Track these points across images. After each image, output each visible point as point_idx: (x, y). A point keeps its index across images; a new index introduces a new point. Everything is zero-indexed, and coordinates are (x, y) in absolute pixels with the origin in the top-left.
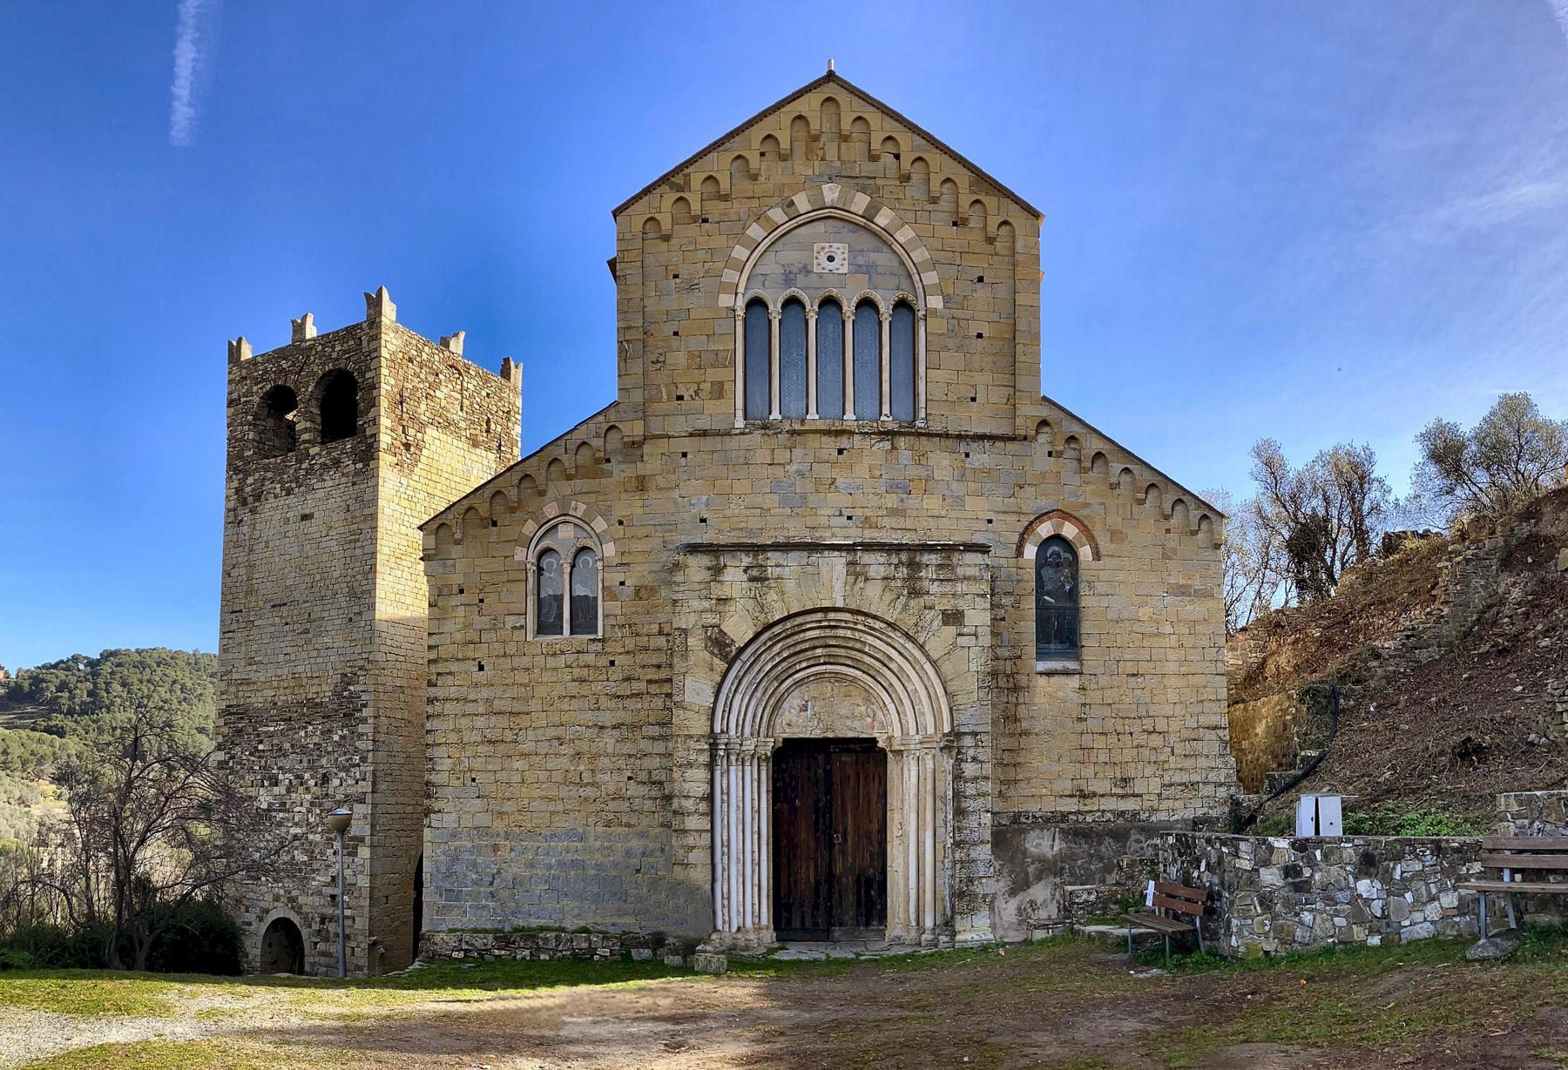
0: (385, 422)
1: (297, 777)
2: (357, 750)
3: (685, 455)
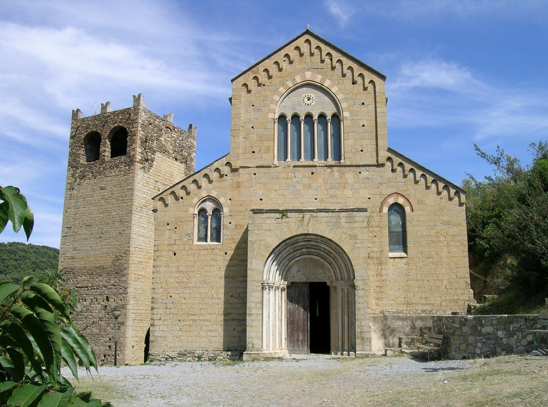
0: (139, 150)
3: (255, 174)
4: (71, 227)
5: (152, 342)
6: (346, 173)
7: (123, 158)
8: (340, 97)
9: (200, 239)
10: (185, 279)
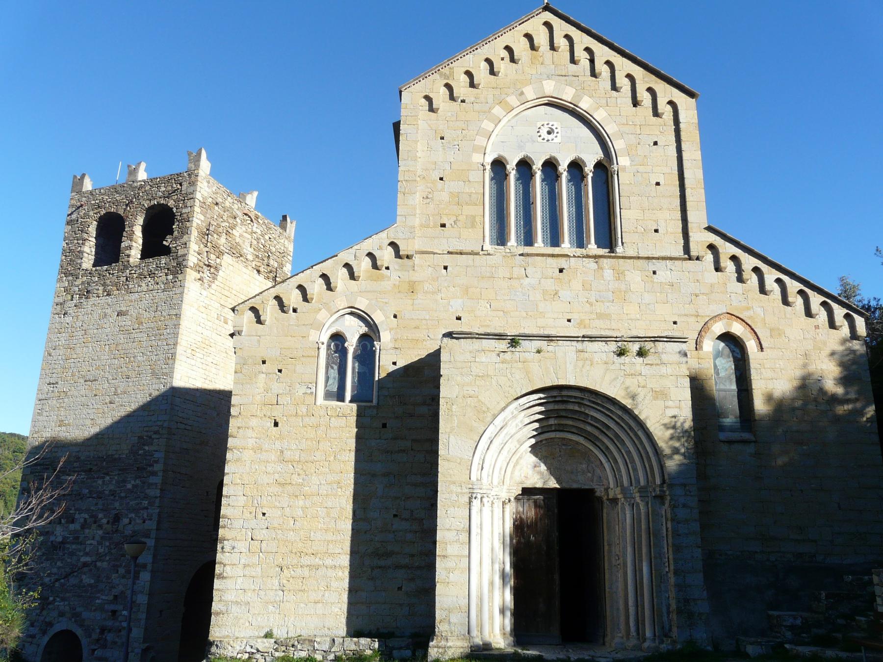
0: (194, 246)
1: (91, 517)
2: (146, 497)
4: (57, 383)
5: (218, 614)
6: (626, 272)
7: (164, 260)
8: (610, 129)
9: (328, 395)
10: (295, 477)
